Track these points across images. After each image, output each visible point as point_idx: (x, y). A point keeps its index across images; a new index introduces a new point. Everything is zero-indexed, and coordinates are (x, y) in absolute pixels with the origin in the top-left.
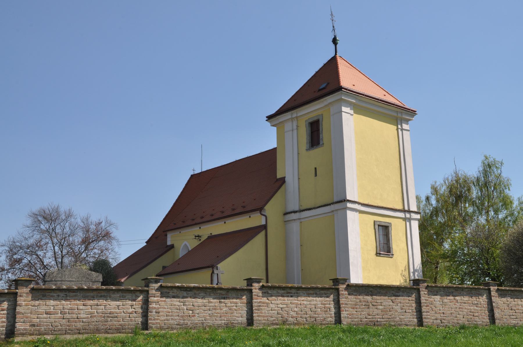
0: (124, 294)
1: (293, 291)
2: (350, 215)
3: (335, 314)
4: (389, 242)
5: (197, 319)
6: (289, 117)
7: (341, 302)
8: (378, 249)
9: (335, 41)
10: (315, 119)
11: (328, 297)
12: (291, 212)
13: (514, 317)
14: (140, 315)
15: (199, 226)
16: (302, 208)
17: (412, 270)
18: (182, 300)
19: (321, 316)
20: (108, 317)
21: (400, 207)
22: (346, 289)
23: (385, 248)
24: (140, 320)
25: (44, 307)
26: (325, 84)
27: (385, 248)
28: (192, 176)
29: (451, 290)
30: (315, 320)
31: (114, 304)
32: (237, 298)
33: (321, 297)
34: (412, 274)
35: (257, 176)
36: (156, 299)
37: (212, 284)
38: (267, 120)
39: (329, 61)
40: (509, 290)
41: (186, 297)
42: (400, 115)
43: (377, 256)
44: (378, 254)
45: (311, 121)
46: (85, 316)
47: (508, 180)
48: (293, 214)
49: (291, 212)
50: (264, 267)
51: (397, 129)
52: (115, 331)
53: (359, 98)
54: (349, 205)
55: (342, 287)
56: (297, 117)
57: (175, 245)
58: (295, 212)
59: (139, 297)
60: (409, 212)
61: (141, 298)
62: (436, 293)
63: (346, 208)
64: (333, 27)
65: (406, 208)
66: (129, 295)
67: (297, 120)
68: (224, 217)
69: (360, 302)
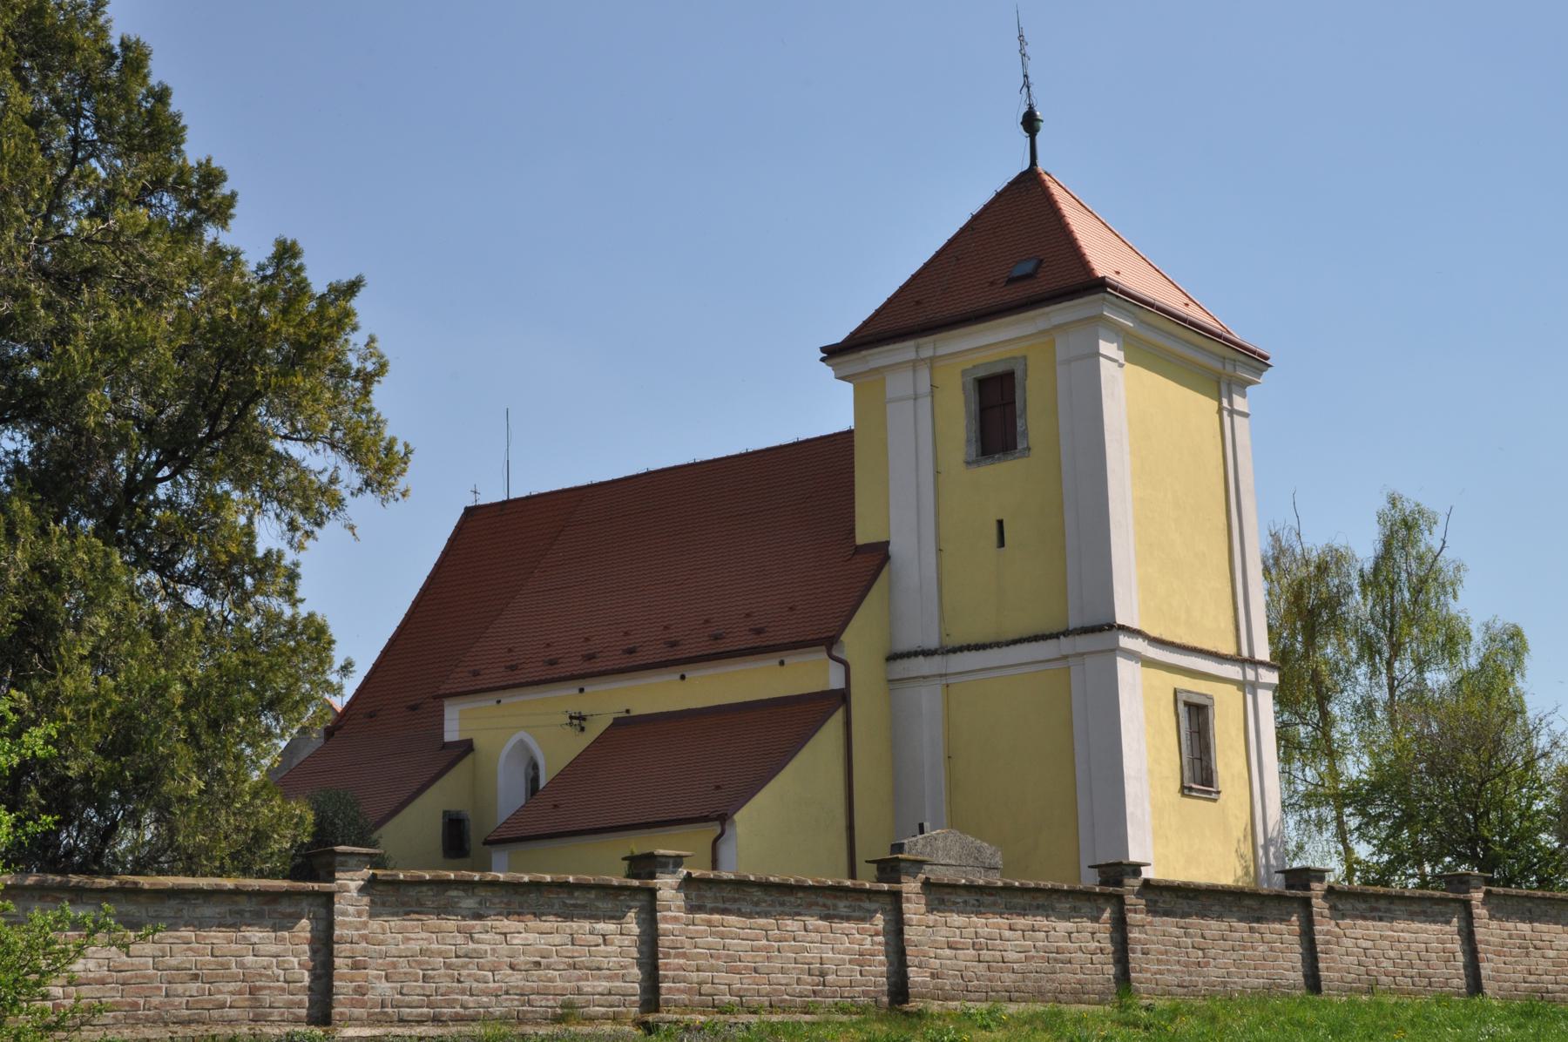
0: (1078, 904)
1: (1382, 904)
2: (1126, 671)
3: (1465, 967)
4: (1208, 752)
5: (1213, 973)
6: (911, 355)
7: (1478, 937)
8: (1187, 774)
9: (1030, 123)
10: (999, 369)
11: (1448, 922)
12: (916, 654)
13: (108, 1017)
14: (1110, 958)
15: (581, 683)
16: (957, 639)
17: (1261, 841)
18: (1182, 922)
19: (1440, 971)
20: (1056, 960)
21: (1228, 648)
22: (1139, 894)
23: (1199, 775)
24: (1111, 970)
25: (944, 931)
26: (1016, 258)
27: (1199, 775)
28: (469, 512)
29: (580, 898)
30: (1430, 984)
31: (1063, 926)
32: (1281, 921)
33: (1435, 922)
34: (1261, 852)
35: (769, 532)
36: (1139, 916)
37: (852, 875)
38: (823, 360)
39: (1011, 184)
40: (237, 892)
41: (1188, 915)
42: (1229, 368)
43: (1183, 795)
44: (1185, 790)
45: (981, 374)
46: (1015, 956)
47: (1458, 569)
48: (921, 658)
49: (916, 654)
50: (842, 823)
51: (1220, 410)
52: (1071, 998)
53: (1142, 314)
54: (1125, 641)
55: (911, 886)
56: (932, 359)
57: (477, 743)
58: (927, 653)
59: (1104, 910)
60: (1253, 663)
61: (1106, 915)
62: (1257, 914)
63: (1115, 650)
64: (1026, 76)
65: (1245, 653)
66: (1086, 907)
67: (931, 368)
68: (676, 660)
69: (1510, 937)
